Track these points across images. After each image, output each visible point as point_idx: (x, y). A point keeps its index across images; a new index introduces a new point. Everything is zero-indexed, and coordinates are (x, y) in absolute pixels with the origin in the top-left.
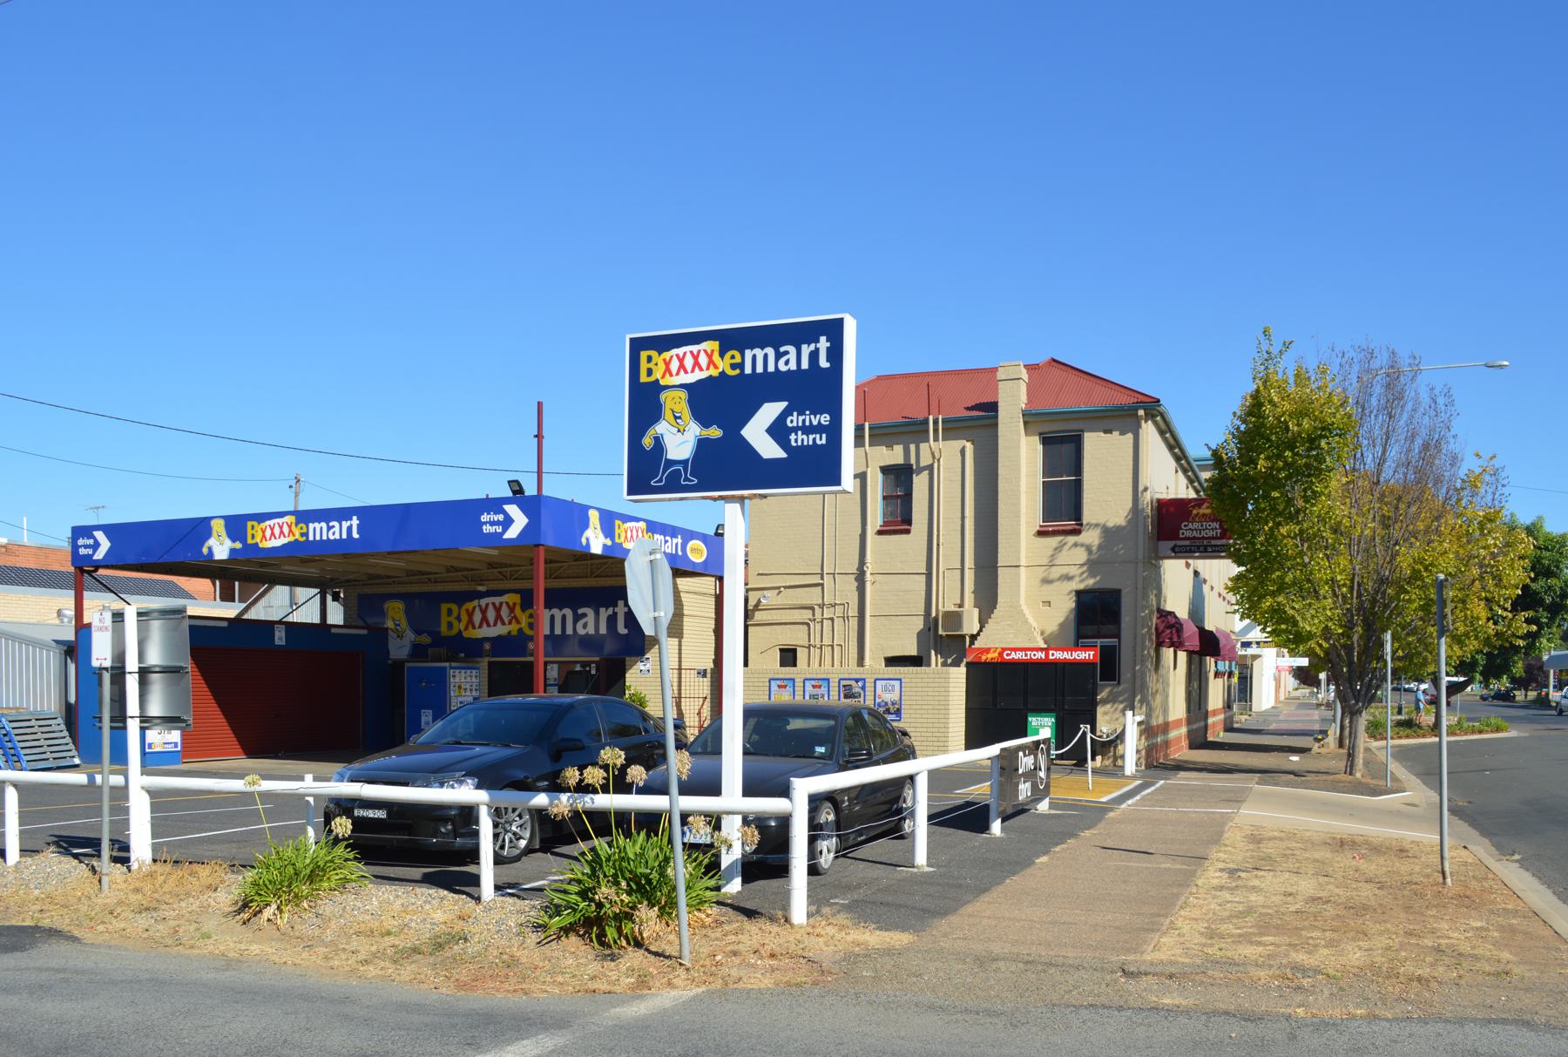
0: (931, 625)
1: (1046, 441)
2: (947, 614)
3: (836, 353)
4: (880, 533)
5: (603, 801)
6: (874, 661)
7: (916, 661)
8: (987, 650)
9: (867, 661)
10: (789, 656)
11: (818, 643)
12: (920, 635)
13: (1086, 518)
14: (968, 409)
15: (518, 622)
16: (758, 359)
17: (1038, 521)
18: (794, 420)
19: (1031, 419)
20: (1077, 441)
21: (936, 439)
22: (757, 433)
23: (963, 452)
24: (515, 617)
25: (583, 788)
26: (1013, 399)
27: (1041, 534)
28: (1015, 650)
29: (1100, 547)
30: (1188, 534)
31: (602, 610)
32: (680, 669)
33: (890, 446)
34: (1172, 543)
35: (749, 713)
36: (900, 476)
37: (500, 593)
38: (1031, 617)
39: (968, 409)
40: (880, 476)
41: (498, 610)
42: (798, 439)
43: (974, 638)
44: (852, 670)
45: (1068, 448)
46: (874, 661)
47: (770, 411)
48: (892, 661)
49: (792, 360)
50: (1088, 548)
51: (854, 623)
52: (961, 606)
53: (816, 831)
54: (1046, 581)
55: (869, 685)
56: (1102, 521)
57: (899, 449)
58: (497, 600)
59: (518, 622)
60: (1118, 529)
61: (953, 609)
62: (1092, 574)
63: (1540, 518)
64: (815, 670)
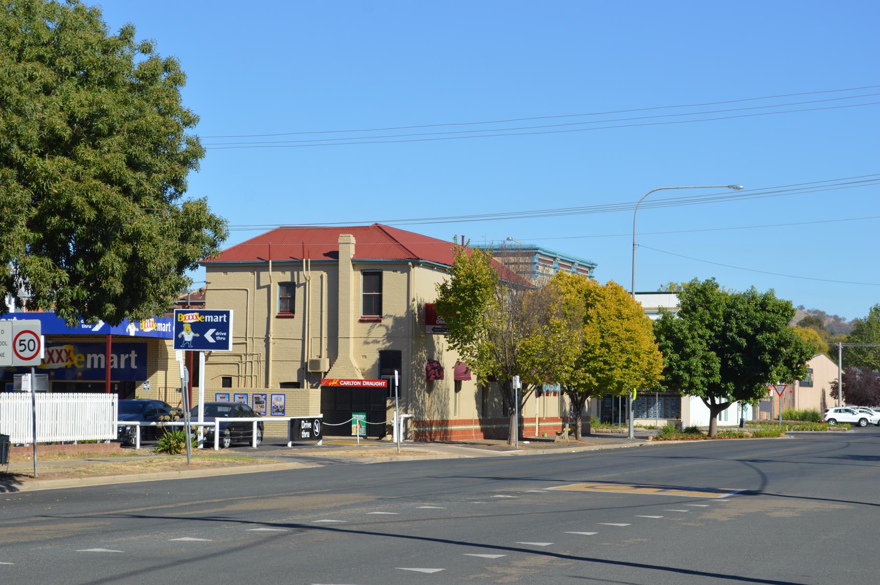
0: (304, 365)
1: (365, 274)
2: (313, 362)
3: (228, 319)
4: (277, 317)
5: (169, 423)
6: (274, 385)
7: (297, 385)
8: (332, 380)
9: (270, 385)
10: (227, 382)
11: (243, 375)
12: (298, 371)
13: (384, 313)
14: (325, 255)
15: (72, 360)
16: (209, 318)
17: (360, 314)
18: (217, 334)
19: (356, 263)
20: (380, 275)
21: (307, 270)
22: (208, 336)
23: (322, 277)
24: (70, 358)
25: (165, 421)
26: (348, 249)
27: (361, 321)
28: (346, 380)
29: (392, 327)
30: (440, 322)
31: (122, 356)
32: (166, 388)
33: (283, 271)
34: (432, 327)
35: (206, 405)
36: (289, 288)
37: (61, 344)
38: (355, 364)
39: (325, 255)
40: (278, 287)
41: (59, 354)
42: (218, 338)
43: (326, 373)
44: (262, 389)
45: (374, 278)
46: (274, 385)
47: (212, 331)
48: (284, 385)
49: (217, 319)
50: (387, 327)
51: (263, 364)
52: (320, 357)
53: (222, 435)
54: (366, 343)
55: (268, 397)
56: (393, 314)
57: (288, 274)
58: (59, 348)
59: (72, 360)
60: (401, 318)
61: (316, 358)
62: (389, 341)
63: (772, 290)
64: (241, 389)
